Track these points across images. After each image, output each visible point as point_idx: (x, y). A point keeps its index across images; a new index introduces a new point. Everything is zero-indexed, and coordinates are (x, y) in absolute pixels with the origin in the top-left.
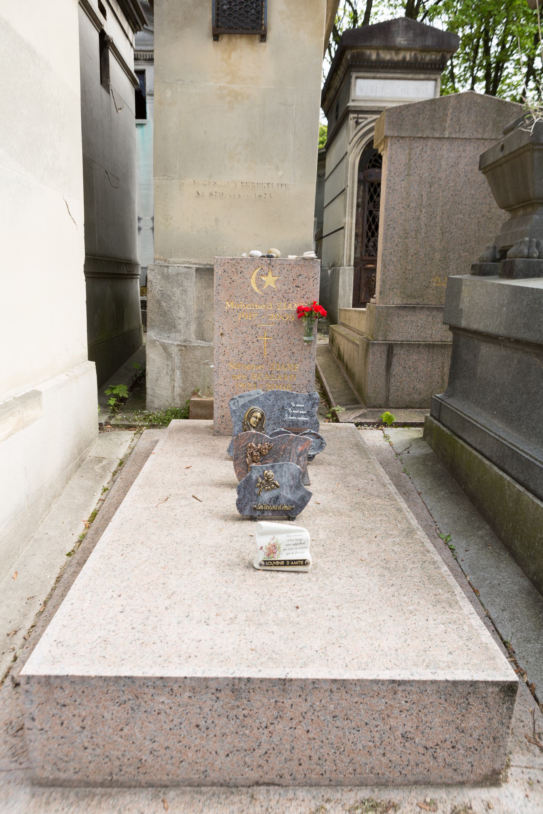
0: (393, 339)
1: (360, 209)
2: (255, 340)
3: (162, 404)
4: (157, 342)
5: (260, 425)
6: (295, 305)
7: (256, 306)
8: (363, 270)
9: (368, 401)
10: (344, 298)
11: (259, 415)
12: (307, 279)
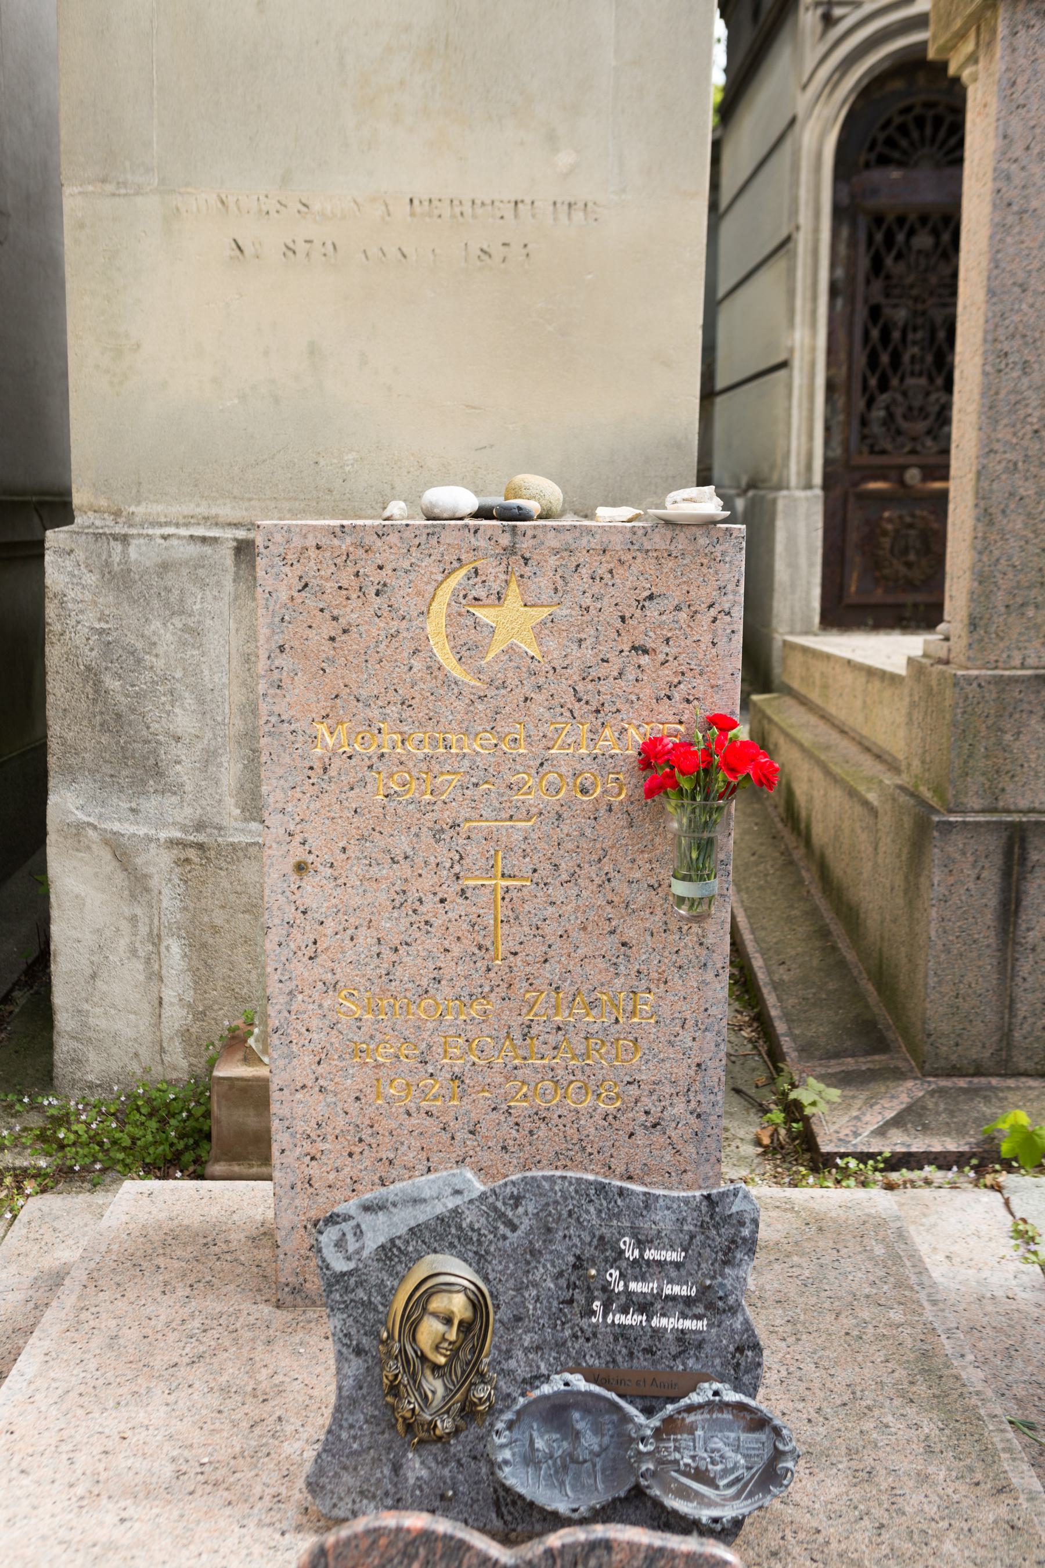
0: (1023, 804)
1: (840, 302)
2: (451, 891)
3: (115, 1067)
4: (90, 832)
5: (465, 1355)
6: (632, 731)
7: (452, 738)
8: (852, 499)
9: (927, 1048)
10: (793, 592)
11: (458, 1305)
12: (683, 616)
